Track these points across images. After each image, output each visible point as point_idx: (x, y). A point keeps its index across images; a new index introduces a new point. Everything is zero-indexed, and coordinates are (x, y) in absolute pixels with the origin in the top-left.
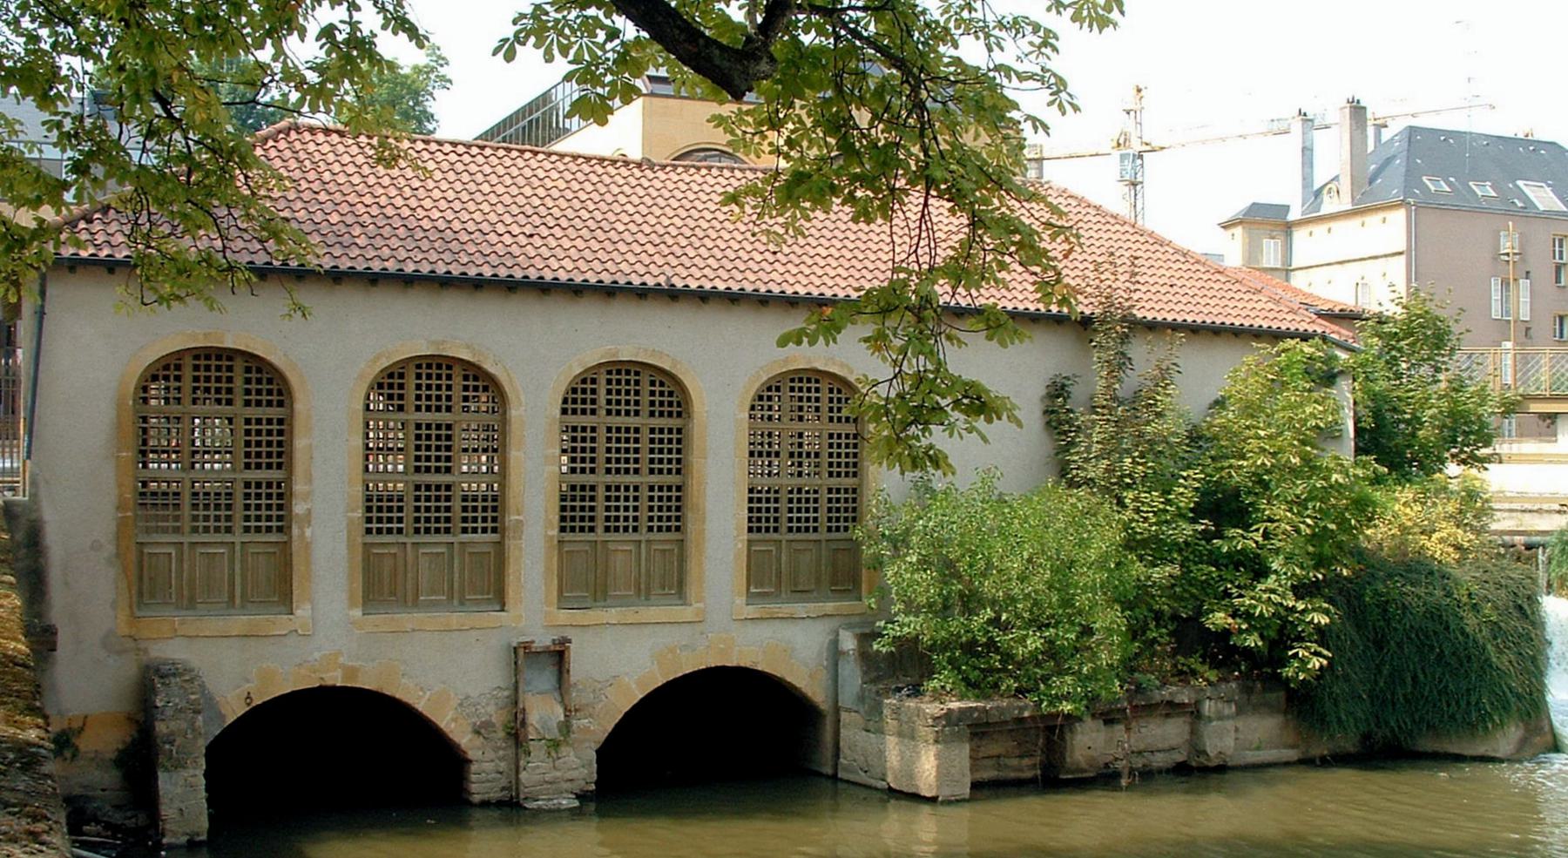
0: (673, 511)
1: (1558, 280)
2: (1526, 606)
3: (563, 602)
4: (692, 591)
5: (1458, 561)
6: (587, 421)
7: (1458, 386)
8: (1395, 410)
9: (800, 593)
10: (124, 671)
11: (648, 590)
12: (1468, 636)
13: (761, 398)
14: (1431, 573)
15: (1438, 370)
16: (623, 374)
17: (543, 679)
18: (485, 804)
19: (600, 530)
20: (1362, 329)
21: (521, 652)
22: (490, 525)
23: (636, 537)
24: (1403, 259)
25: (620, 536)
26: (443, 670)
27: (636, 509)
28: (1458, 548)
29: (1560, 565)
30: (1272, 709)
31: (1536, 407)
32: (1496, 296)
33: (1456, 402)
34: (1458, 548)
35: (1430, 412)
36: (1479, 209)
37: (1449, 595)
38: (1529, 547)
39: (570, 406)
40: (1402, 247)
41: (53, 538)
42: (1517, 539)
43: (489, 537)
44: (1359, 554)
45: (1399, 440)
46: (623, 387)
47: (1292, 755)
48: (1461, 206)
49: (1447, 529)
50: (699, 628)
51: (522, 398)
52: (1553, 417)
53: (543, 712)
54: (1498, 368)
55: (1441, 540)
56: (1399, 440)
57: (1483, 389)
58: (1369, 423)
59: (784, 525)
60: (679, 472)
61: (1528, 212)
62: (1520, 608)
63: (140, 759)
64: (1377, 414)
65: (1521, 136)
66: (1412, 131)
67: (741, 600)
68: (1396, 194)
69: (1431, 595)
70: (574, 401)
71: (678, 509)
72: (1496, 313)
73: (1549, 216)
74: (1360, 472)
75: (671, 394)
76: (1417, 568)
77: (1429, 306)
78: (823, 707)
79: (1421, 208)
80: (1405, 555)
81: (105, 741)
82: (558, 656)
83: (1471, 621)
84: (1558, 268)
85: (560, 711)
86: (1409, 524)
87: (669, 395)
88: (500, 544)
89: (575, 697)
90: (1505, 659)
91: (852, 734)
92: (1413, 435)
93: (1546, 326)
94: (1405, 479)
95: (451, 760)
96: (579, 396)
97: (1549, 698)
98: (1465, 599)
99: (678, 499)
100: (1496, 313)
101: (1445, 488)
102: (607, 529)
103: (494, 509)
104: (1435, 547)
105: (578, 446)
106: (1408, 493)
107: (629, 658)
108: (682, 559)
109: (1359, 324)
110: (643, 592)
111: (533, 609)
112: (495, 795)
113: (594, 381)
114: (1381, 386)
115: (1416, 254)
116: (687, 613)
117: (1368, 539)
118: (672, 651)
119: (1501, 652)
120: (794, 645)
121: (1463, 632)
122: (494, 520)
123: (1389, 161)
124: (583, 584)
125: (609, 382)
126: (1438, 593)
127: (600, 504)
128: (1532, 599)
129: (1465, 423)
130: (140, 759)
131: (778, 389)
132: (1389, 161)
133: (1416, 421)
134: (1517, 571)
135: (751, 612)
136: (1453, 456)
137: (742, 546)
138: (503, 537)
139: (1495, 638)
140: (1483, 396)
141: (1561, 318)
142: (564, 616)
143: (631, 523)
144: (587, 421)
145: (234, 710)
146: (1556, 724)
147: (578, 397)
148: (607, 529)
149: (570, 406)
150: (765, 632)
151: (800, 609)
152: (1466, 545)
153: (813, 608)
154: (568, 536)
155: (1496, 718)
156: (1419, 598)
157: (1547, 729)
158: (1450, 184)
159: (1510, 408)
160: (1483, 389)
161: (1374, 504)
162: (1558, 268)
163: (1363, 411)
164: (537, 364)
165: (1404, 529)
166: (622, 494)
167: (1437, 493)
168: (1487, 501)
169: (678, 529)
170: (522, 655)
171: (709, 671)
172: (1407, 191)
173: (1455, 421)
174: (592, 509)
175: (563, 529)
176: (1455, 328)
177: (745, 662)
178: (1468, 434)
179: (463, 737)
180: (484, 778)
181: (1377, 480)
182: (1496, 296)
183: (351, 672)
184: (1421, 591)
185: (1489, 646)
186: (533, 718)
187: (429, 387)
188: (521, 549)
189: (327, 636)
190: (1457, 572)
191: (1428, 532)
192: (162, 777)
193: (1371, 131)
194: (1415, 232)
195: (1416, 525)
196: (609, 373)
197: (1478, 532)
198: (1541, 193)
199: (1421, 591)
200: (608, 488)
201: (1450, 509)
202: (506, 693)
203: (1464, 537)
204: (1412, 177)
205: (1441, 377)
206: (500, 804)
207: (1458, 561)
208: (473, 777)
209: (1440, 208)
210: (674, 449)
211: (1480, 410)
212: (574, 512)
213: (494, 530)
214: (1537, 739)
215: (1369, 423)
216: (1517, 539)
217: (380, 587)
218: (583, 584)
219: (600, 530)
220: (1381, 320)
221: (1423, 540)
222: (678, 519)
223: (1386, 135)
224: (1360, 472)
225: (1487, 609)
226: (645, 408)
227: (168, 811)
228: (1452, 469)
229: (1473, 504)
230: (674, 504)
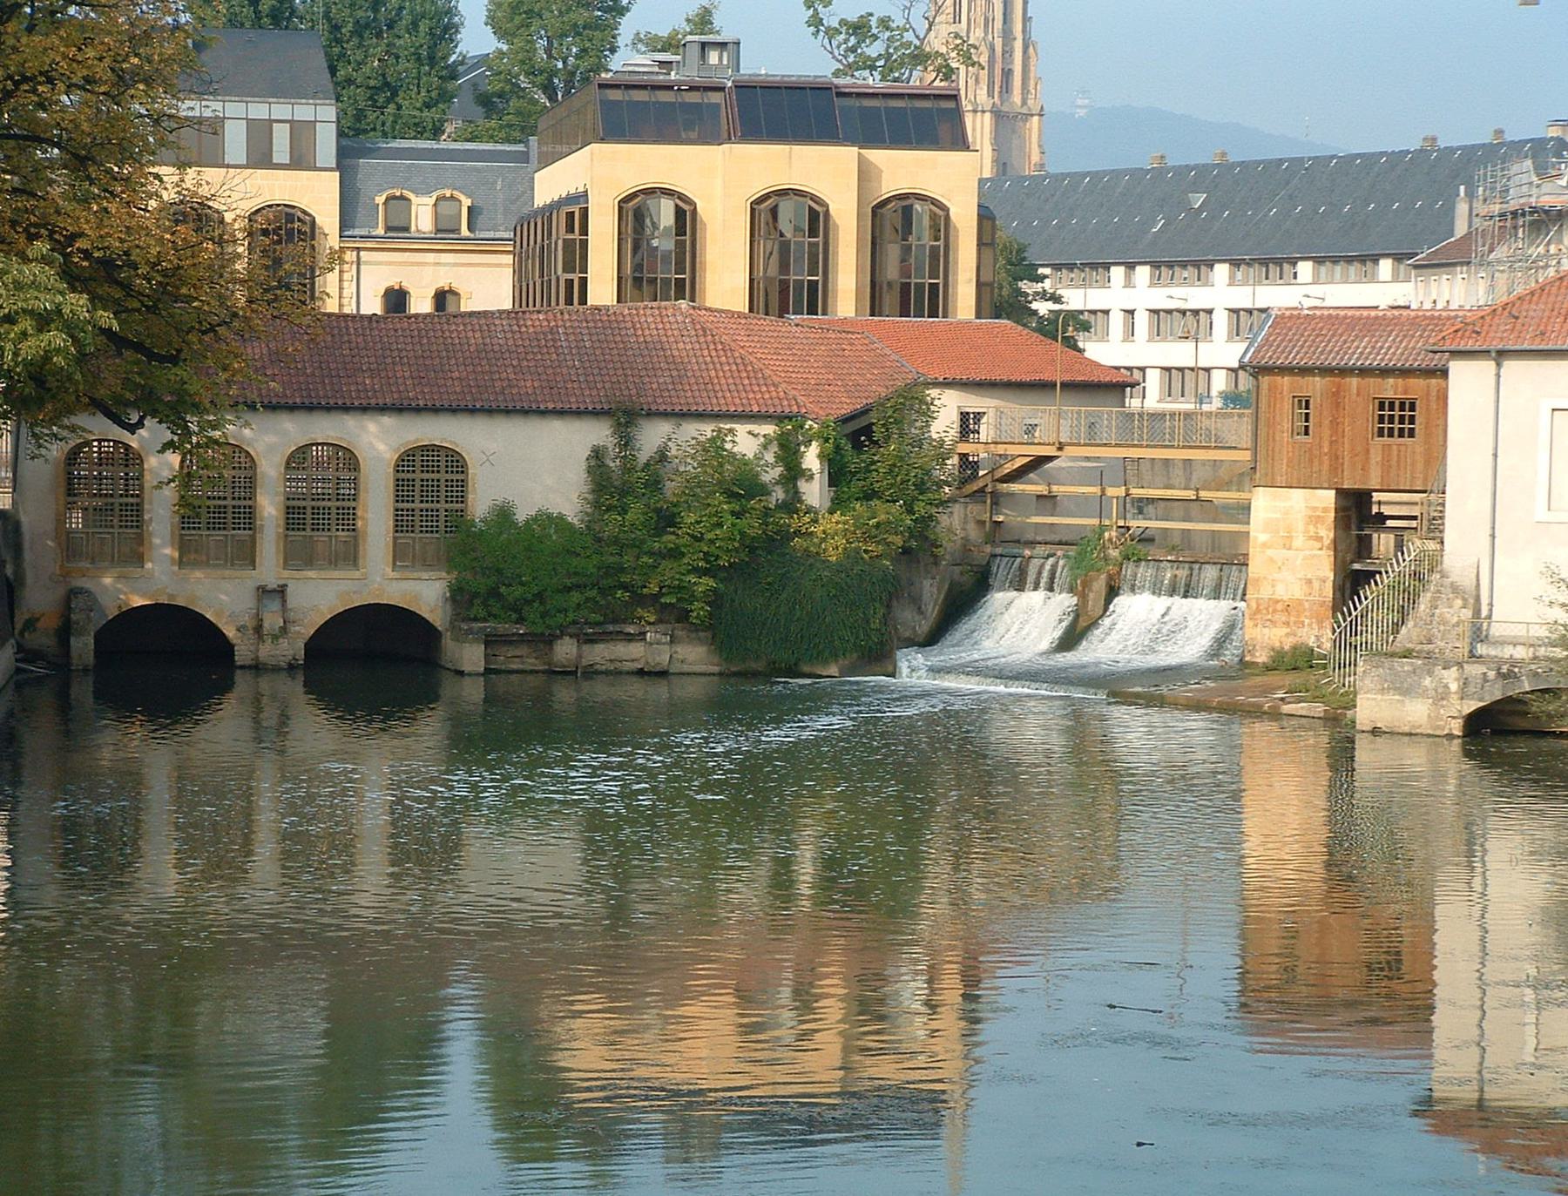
3: (286, 566)
4: (361, 562)
9: (428, 566)
10: (61, 592)
17: (275, 605)
18: (242, 667)
26: (221, 598)
30: (701, 641)
41: (25, 528)
47: (716, 669)
53: (272, 621)
59: (418, 529)
63: (65, 631)
67: (389, 570)
78: (438, 624)
81: (50, 623)
82: (281, 591)
88: (355, 538)
91: (448, 643)
95: (227, 648)
107: (321, 597)
108: (356, 546)
111: (269, 566)
112: (248, 662)
116: (357, 574)
120: (425, 594)
124: (298, 556)
127: (309, 516)
130: (65, 631)
135: (395, 575)
137: (390, 540)
142: (286, 573)
145: (112, 613)
150: (405, 585)
151: (425, 575)
153: (434, 575)
170: (263, 592)
179: (230, 632)
180: (242, 654)
183: (171, 596)
186: (266, 625)
189: (159, 576)
192: (72, 640)
206: (250, 667)
217: (189, 553)
218: (298, 556)
227: (74, 653)
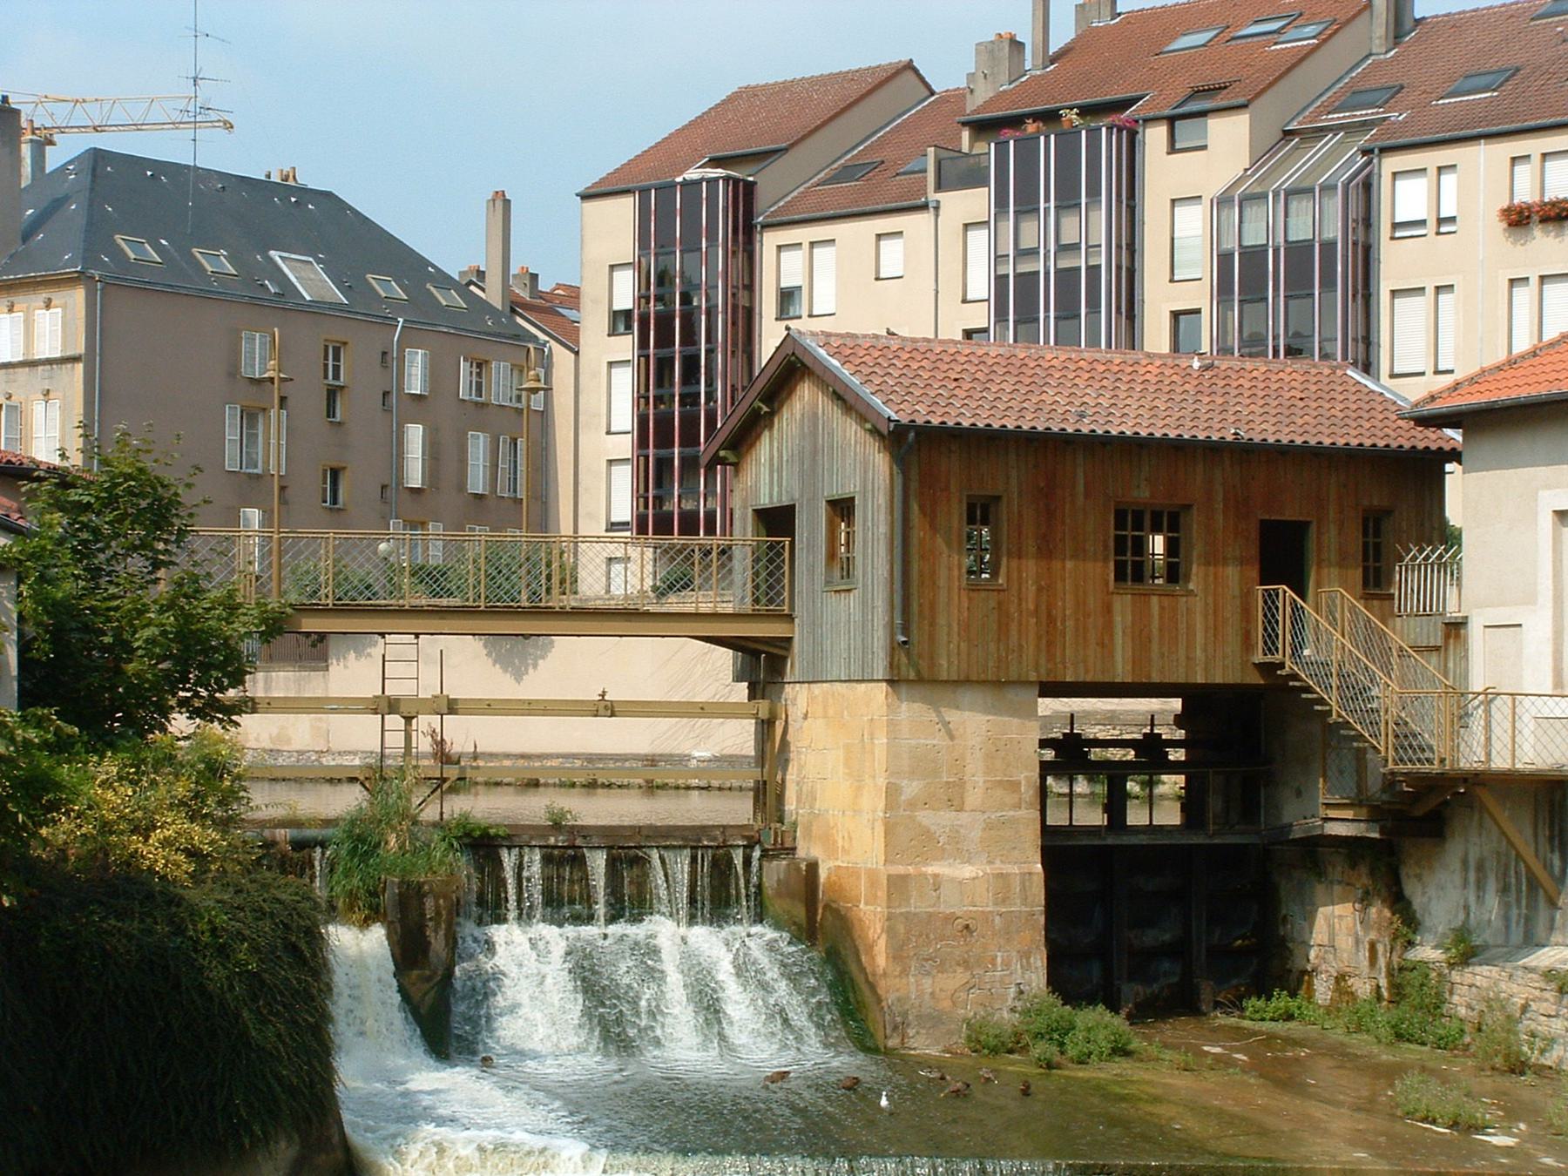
1: (331, 412)
2: (303, 946)
5: (192, 876)
7: (191, 588)
8: (86, 628)
12: (211, 998)
14: (150, 896)
15: (157, 565)
20: (32, 496)
24: (80, 367)
28: (192, 853)
29: (348, 874)
31: (311, 624)
32: (232, 435)
33: (187, 618)
34: (192, 853)
35: (148, 633)
36: (207, 293)
37: (180, 930)
38: (300, 845)
40: (80, 349)
42: (281, 834)
44: (29, 869)
45: (95, 679)
48: (177, 287)
49: (173, 825)
52: (322, 637)
54: (244, 550)
55: (166, 843)
56: (95, 679)
57: (231, 595)
58: (44, 651)
61: (285, 303)
62: (294, 949)
64: (57, 635)
65: (276, 178)
66: (98, 158)
68: (69, 261)
69: (150, 932)
72: (231, 462)
73: (318, 310)
74: (32, 734)
76: (121, 887)
77: (148, 463)
79: (112, 290)
80: (106, 867)
83: (217, 973)
84: (332, 394)
86: (112, 816)
90: (270, 1032)
92: (118, 671)
93: (311, 484)
94: (103, 742)
97: (339, 1090)
98: (206, 938)
100: (231, 462)
101: (170, 758)
104: (153, 853)
106: (110, 767)
109: (25, 487)
114: (66, 589)
115: (104, 364)
117: (45, 842)
119: (264, 1021)
121: (202, 990)
123: (58, 204)
126: (162, 928)
128: (315, 939)
129: (204, 652)
132: (58, 204)
133: (124, 647)
134: (286, 888)
136: (183, 703)
139: (255, 999)
140: (231, 607)
141: (335, 473)
146: (348, 1129)
152: (207, 849)
155: (257, 1129)
156: (129, 937)
157: (336, 1139)
158: (159, 249)
159: (274, 627)
160: (231, 595)
161: (58, 786)
162: (332, 394)
163: (31, 630)
165: (106, 827)
167: (157, 766)
168: (239, 777)
172: (90, 258)
173: (187, 648)
176: (186, 496)
178: (208, 664)
181: (60, 747)
182: (232, 435)
184: (134, 926)
185: (245, 1014)
190: (193, 895)
191: (145, 830)
193: (26, 150)
194: (99, 326)
195: (122, 817)
197: (225, 824)
198: (306, 272)
199: (134, 926)
201: (180, 790)
203: (203, 836)
204: (96, 236)
205: (161, 573)
207: (192, 876)
209: (144, 289)
211: (227, 630)
214: (321, 1159)
215: (44, 651)
216: (281, 834)
220: (64, 479)
221: (136, 842)
223: (55, 158)
224: (32, 734)
225: (242, 951)
228: (180, 723)
229: (217, 777)
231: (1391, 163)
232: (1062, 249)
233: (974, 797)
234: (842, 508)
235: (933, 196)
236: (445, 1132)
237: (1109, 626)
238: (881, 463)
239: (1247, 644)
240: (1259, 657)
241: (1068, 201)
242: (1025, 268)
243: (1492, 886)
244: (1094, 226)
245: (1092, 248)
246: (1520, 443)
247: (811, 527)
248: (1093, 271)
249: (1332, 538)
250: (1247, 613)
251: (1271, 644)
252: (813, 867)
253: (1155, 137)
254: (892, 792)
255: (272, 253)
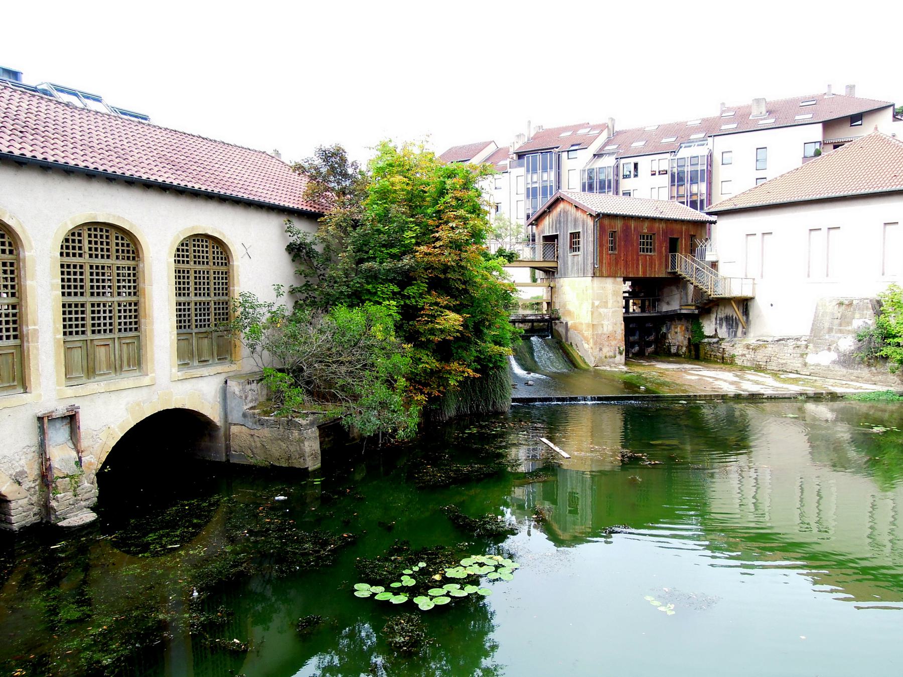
0: (132, 320)
6: (77, 260)
11: (121, 367)
13: (73, 234)
16: (98, 229)
17: (58, 436)
19: (89, 332)
21: (46, 420)
22: (12, 333)
23: (112, 336)
25: (102, 336)
27: (110, 318)
39: (65, 251)
43: (12, 342)
46: (99, 240)
50: (153, 387)
51: (33, 244)
53: (61, 455)
60: (135, 294)
67: (175, 370)
70: (67, 247)
71: (136, 317)
75: (128, 245)
78: (218, 424)
82: (71, 419)
85: (74, 454)
87: (128, 244)
88: (21, 346)
89: (84, 443)
96: (71, 244)
99: (136, 311)
102: (93, 332)
103: (15, 322)
105: (70, 279)
108: (139, 348)
110: (116, 367)
111: (48, 388)
113: (79, 235)
116: (146, 381)
118: (138, 405)
122: (15, 329)
124: (82, 367)
125: (90, 236)
131: (187, 245)
138: (22, 342)
142: (70, 392)
143: (108, 327)
144: (77, 260)
147: (71, 244)
148: (93, 332)
149: (65, 251)
150: (188, 386)
151: (205, 371)
154: (69, 338)
164: (160, 229)
166: (102, 308)
169: (136, 329)
171: (159, 413)
174: (83, 319)
175: (65, 334)
177: (179, 405)
186: (56, 463)
187: (98, 281)
188: (37, 349)
196: (194, 240)
200: (93, 305)
202: (33, 449)
208: (13, 512)
210: (133, 281)
212: (73, 321)
213: (15, 337)
218: (82, 367)
219: (89, 332)
222: (136, 323)
226: (113, 254)
230: (133, 314)
231: (623, 161)
232: (543, 181)
233: (610, 305)
234: (575, 235)
235: (509, 170)
236: (896, 340)
237: (638, 265)
238: (590, 222)
239: (667, 267)
240: (669, 270)
241: (545, 169)
242: (534, 186)
243: (724, 324)
244: (553, 175)
245: (551, 181)
246: (847, 203)
247: (564, 242)
248: (551, 186)
249: (683, 243)
250: (667, 261)
251: (673, 267)
252: (567, 323)
253: (564, 155)
254: (593, 304)
255: (643, 143)
